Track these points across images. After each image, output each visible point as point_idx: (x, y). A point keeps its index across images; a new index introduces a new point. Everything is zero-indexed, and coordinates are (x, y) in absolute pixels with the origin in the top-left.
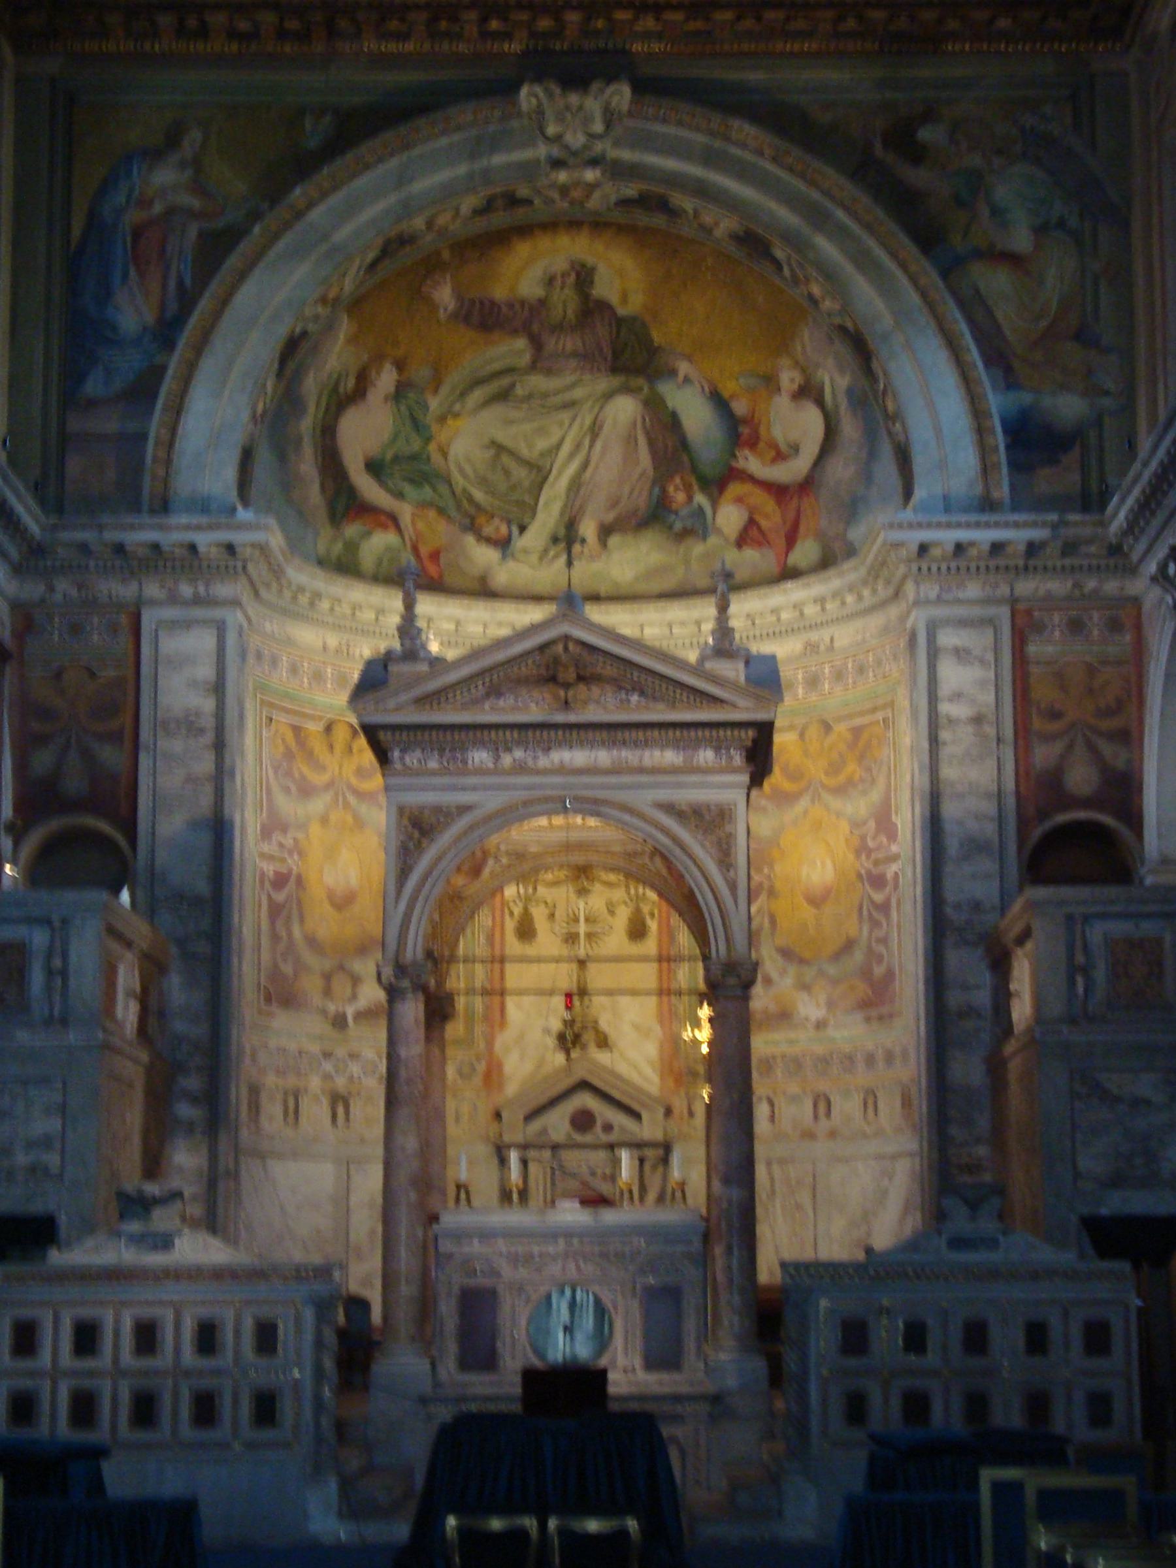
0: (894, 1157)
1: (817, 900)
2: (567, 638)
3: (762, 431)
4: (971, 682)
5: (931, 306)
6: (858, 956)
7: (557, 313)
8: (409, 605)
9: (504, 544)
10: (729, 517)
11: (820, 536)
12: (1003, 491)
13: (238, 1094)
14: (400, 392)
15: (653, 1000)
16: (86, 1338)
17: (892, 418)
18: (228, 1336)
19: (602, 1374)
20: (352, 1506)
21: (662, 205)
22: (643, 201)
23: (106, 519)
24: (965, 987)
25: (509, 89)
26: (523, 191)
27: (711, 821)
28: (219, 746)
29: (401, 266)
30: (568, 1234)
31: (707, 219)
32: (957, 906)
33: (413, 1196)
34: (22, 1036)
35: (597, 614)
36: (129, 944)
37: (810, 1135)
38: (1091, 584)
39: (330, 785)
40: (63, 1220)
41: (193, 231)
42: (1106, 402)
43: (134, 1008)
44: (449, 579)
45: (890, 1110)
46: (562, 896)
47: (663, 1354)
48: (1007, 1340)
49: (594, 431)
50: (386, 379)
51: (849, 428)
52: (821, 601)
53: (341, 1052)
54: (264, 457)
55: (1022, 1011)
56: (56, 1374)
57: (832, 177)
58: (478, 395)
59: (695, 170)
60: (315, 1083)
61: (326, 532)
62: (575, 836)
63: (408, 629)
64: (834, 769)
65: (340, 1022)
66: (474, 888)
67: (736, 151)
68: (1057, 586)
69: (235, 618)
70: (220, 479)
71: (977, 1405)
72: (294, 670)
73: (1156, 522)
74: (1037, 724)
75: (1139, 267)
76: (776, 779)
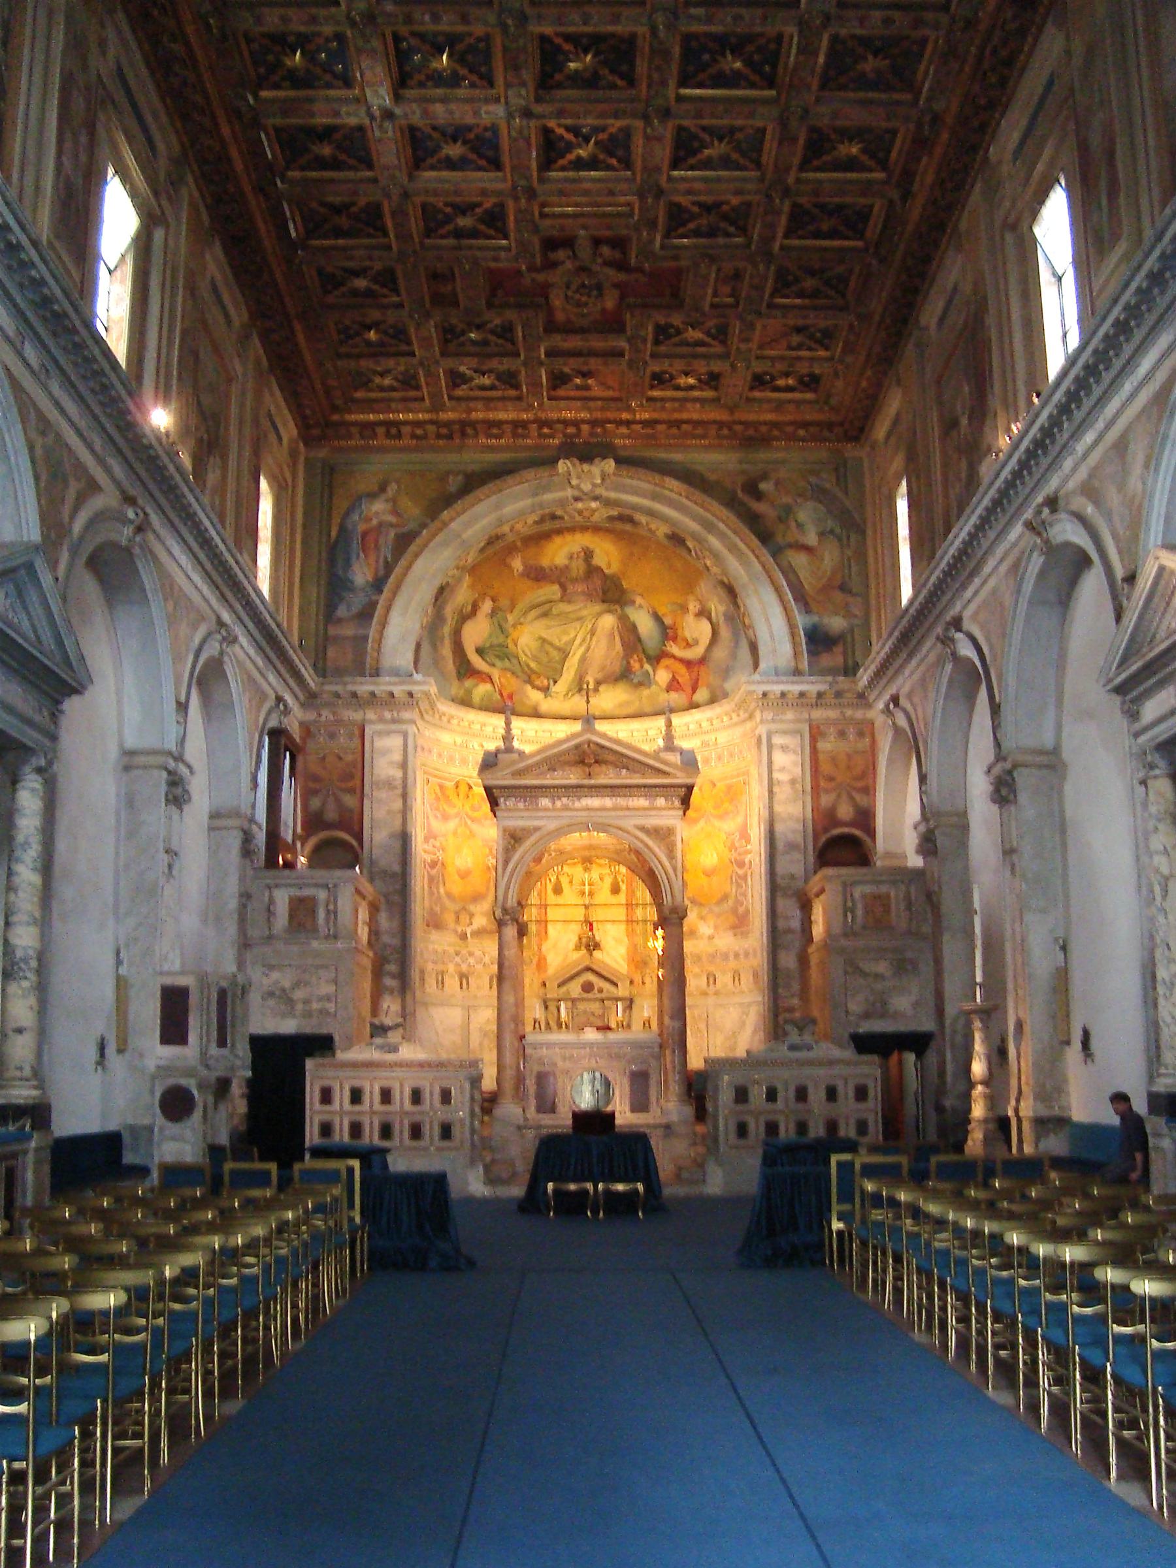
0: (750, 1005)
1: (708, 874)
2: (589, 742)
3: (679, 632)
4: (790, 763)
5: (767, 572)
6: (730, 902)
7: (574, 573)
8: (508, 724)
9: (546, 690)
10: (662, 676)
11: (708, 686)
12: (804, 665)
13: (415, 975)
14: (493, 613)
15: (623, 927)
16: (356, 1096)
17: (750, 627)
18: (426, 1095)
19: (612, 1116)
20: (491, 1180)
21: (630, 520)
22: (621, 518)
23: (348, 679)
24: (787, 918)
25: (554, 462)
26: (559, 513)
27: (664, 835)
28: (405, 796)
29: (497, 550)
30: (591, 1045)
31: (653, 527)
32: (783, 878)
33: (512, 1026)
34: (315, 944)
35: (601, 726)
36: (364, 898)
37: (705, 994)
38: (849, 713)
39: (458, 815)
40: (336, 1038)
41: (392, 535)
42: (856, 621)
43: (366, 929)
44: (518, 708)
45: (747, 980)
46: (577, 872)
47: (640, 1104)
48: (817, 1096)
49: (593, 633)
50: (487, 606)
51: (725, 633)
52: (710, 720)
53: (464, 952)
54: (426, 648)
55: (818, 930)
56: (342, 1113)
57: (716, 506)
58: (533, 613)
59: (646, 502)
60: (451, 968)
61: (456, 683)
62: (594, 842)
63: (508, 737)
64: (717, 807)
65: (464, 937)
66: (537, 869)
67: (667, 492)
68: (832, 714)
69: (412, 729)
70: (404, 659)
71: (802, 1128)
72: (440, 755)
73: (884, 680)
74: (822, 783)
75: (871, 553)
76: (690, 813)
